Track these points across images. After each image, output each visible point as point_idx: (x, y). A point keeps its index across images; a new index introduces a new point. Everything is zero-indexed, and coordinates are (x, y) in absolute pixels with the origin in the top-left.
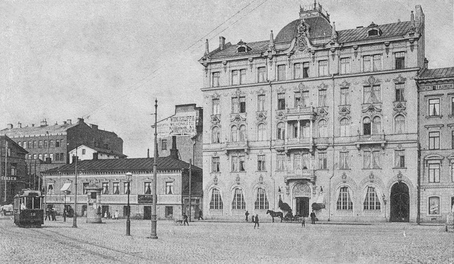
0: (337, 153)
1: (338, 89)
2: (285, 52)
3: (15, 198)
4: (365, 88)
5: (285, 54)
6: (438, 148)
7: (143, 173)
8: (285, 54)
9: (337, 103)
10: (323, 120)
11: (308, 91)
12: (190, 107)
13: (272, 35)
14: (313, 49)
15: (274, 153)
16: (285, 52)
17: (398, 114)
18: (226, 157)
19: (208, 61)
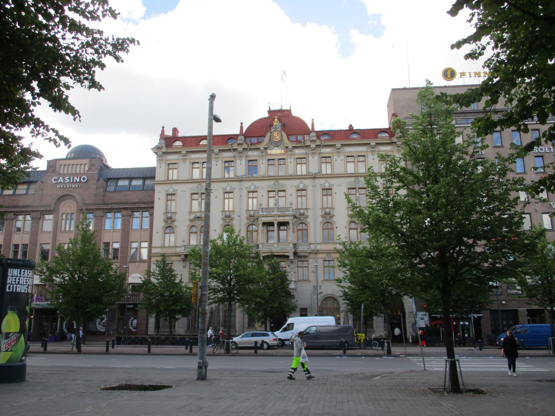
0: (320, 263)
1: (319, 192)
2: (258, 146)
3: (97, 266)
4: (349, 190)
5: (259, 149)
6: (351, 231)
7: (351, 213)
8: (259, 149)
9: (319, 206)
10: (170, 227)
11: (284, 191)
12: (200, 208)
13: (242, 128)
14: (290, 146)
15: (364, 196)
16: (258, 146)
17: (300, 222)
18: (182, 264)
19: (164, 150)
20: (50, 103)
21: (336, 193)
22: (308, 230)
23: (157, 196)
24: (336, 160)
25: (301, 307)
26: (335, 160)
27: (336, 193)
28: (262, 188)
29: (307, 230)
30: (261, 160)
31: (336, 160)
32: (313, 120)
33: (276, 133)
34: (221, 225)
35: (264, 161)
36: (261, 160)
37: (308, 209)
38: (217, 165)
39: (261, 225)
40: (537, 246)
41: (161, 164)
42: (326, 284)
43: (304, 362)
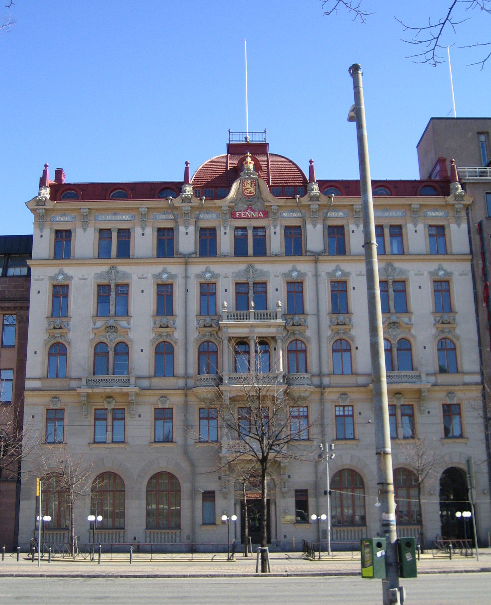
20: (42, 177)
21: (354, 288)
22: (308, 351)
23: (34, 286)
24: (353, 232)
25: (297, 488)
26: (351, 232)
27: (354, 288)
28: (226, 277)
29: (305, 351)
30: (222, 229)
31: (353, 232)
32: (311, 162)
33: (249, 182)
34: (91, 341)
35: (228, 230)
36: (222, 229)
37: (308, 314)
38: (143, 234)
39: (226, 342)
40: (175, 197)
41: (41, 230)
42: (205, 528)
43: (415, 464)
